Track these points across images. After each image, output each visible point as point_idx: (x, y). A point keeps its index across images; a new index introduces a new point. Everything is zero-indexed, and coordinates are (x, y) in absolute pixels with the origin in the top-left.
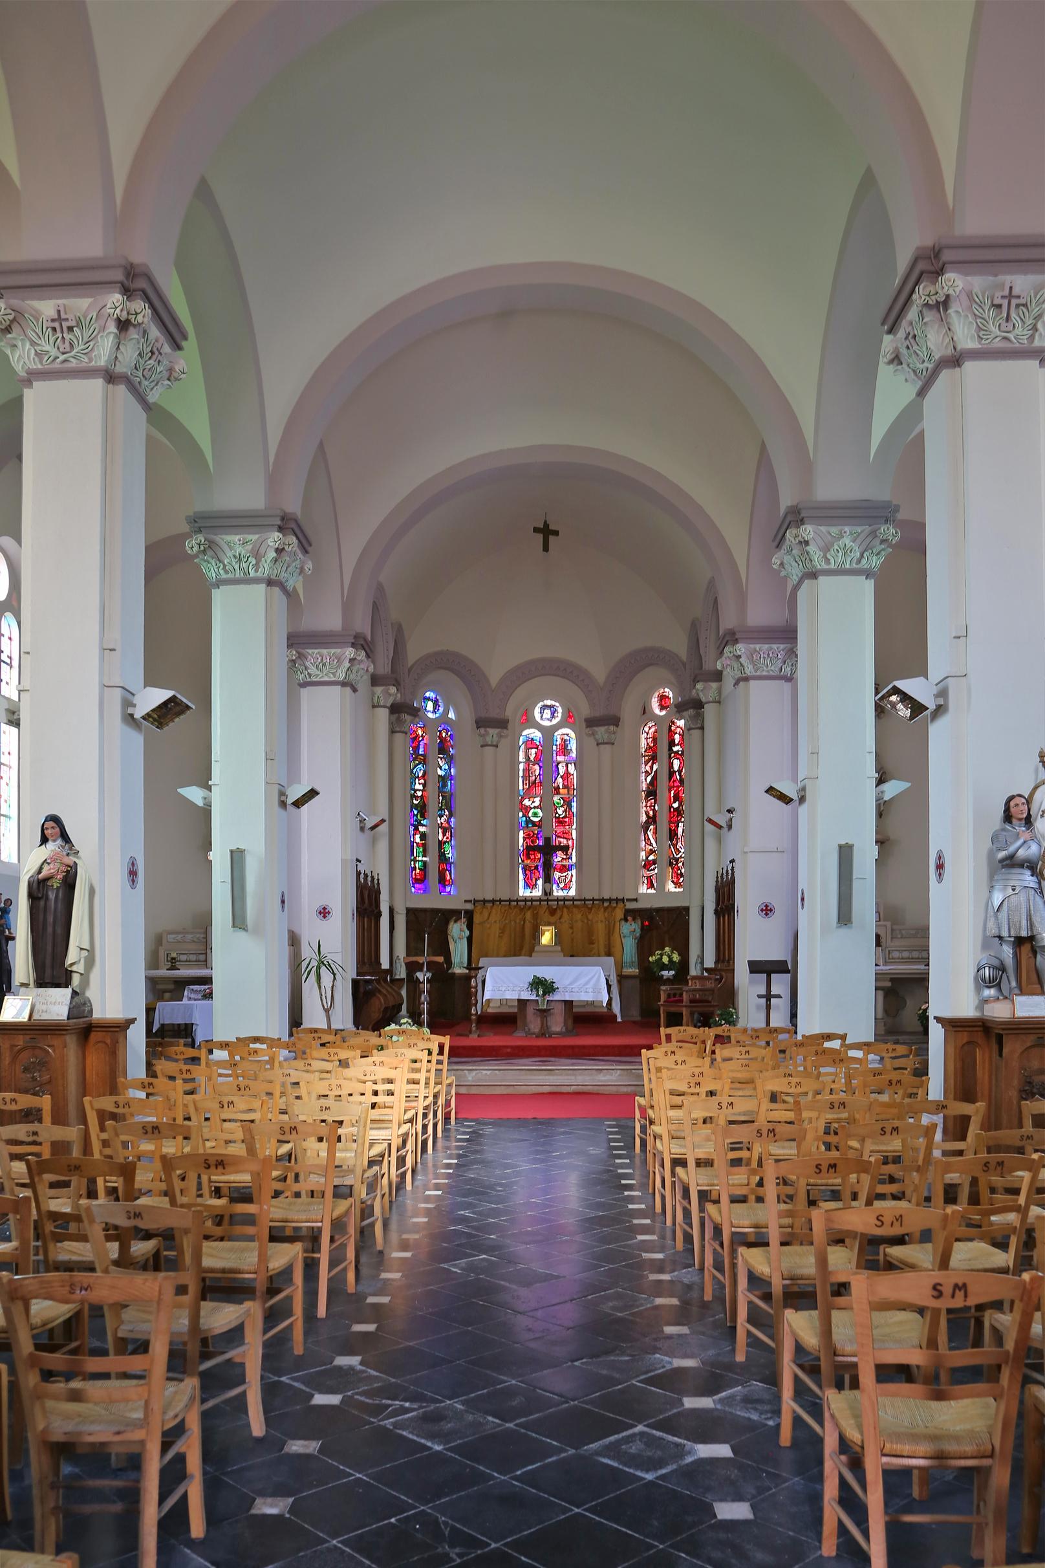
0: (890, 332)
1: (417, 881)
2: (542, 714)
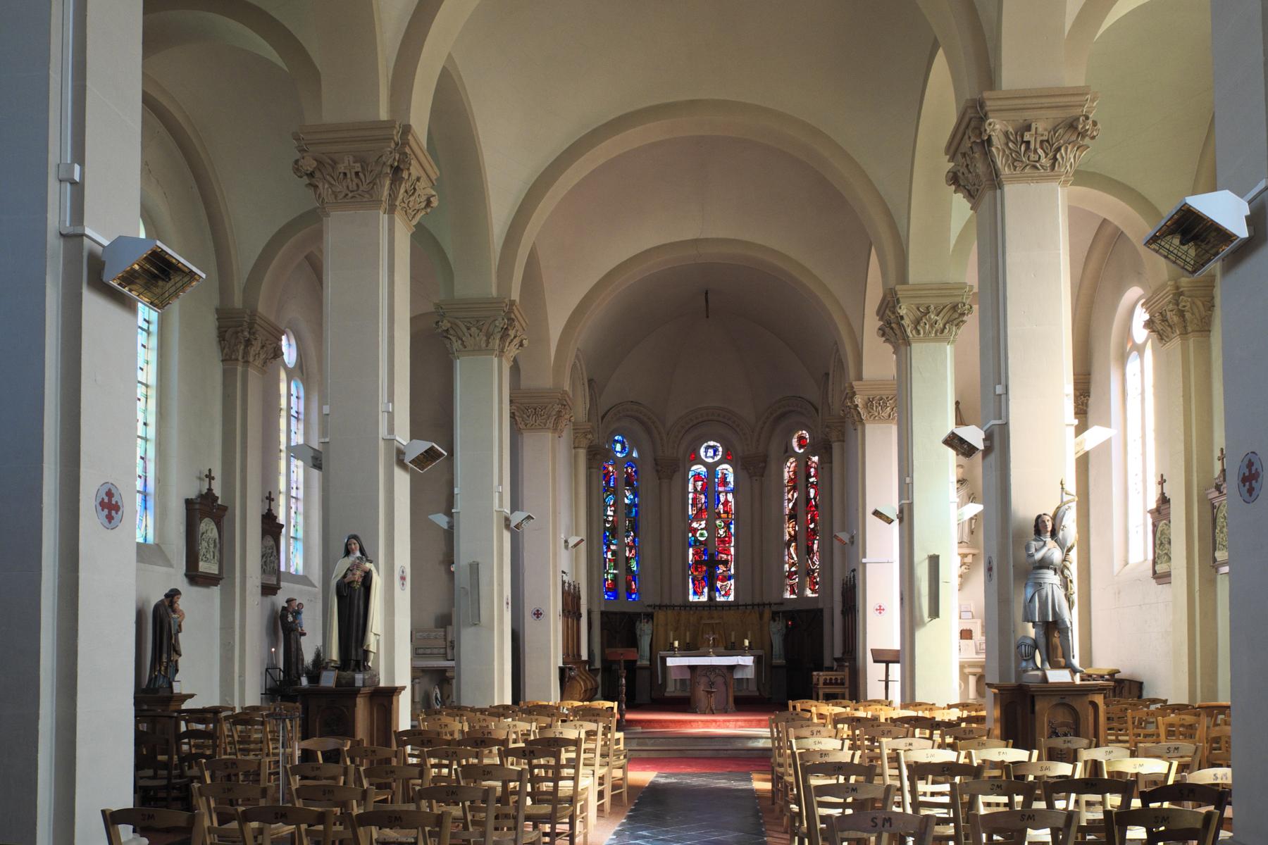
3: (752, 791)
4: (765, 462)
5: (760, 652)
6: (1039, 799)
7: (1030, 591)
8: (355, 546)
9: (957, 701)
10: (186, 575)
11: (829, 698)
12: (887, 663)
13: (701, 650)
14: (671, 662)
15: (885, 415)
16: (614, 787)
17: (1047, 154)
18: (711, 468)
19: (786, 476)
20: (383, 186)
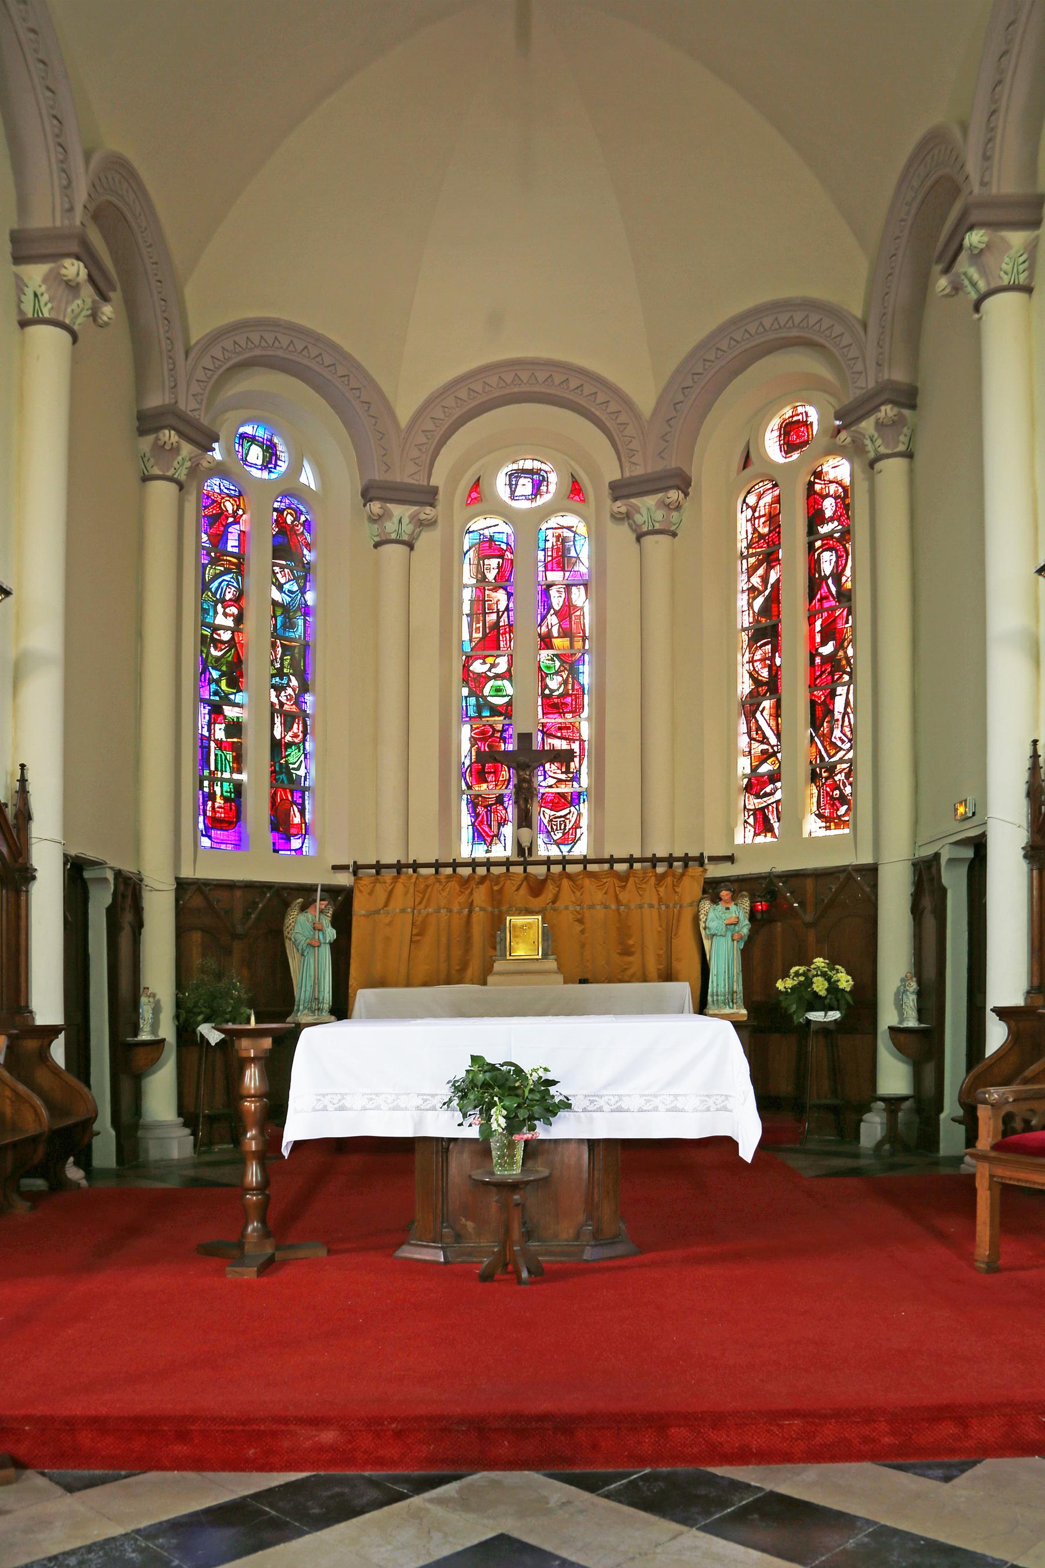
0: (947, 270)
1: (214, 823)
2: (512, 487)
10: (737, 1144)
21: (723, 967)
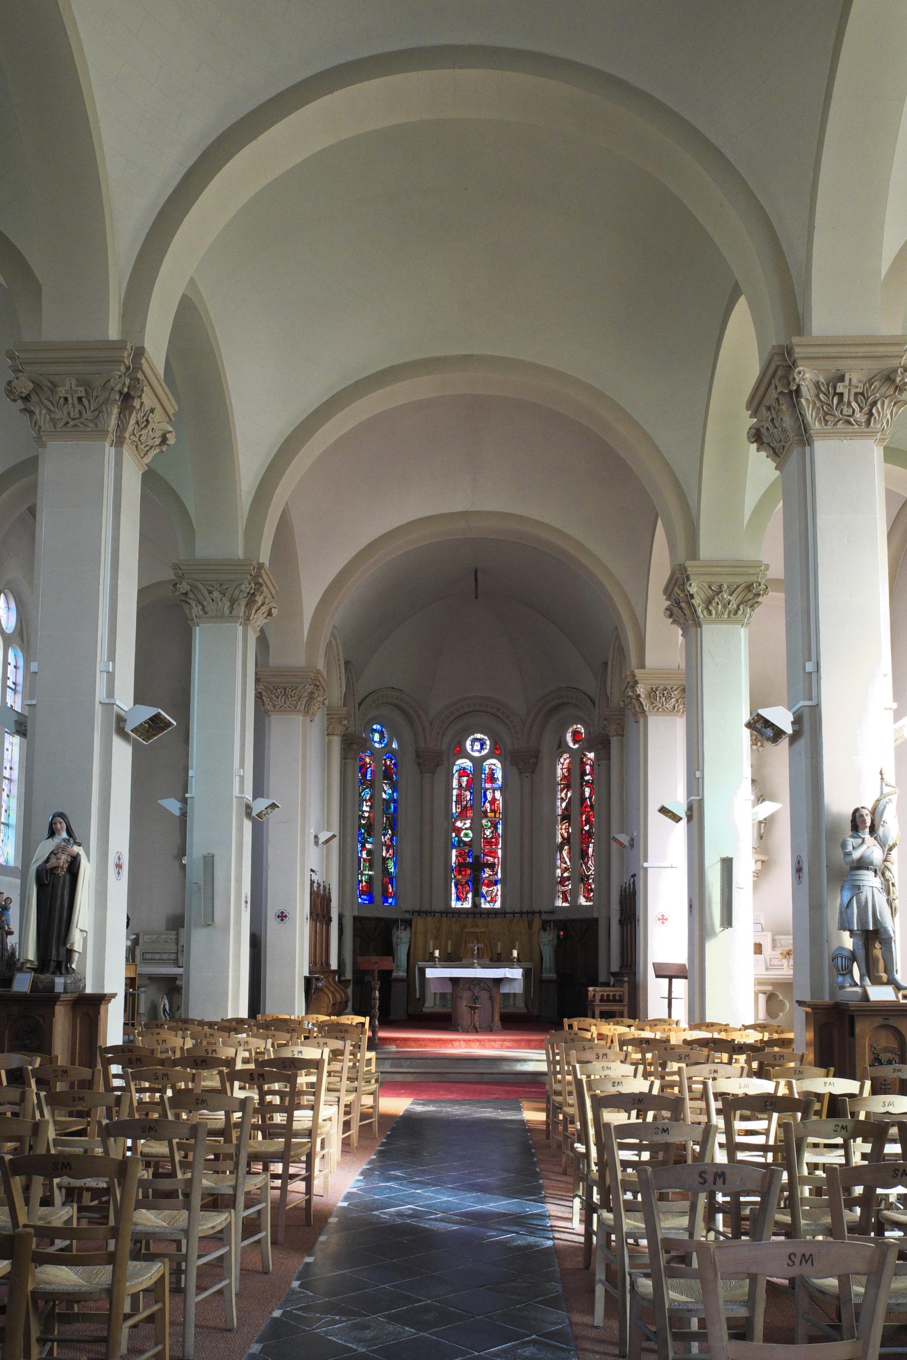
2: (472, 745)
3: (522, 1122)
4: (537, 757)
5: (529, 965)
6: (894, 1141)
7: (847, 895)
8: (61, 826)
9: (752, 1022)
11: (607, 1016)
12: (670, 978)
13: (464, 962)
14: (430, 973)
15: (669, 706)
16: (364, 1116)
17: (861, 409)
18: (478, 763)
19: (559, 773)
20: (109, 414)
21: (548, 958)
